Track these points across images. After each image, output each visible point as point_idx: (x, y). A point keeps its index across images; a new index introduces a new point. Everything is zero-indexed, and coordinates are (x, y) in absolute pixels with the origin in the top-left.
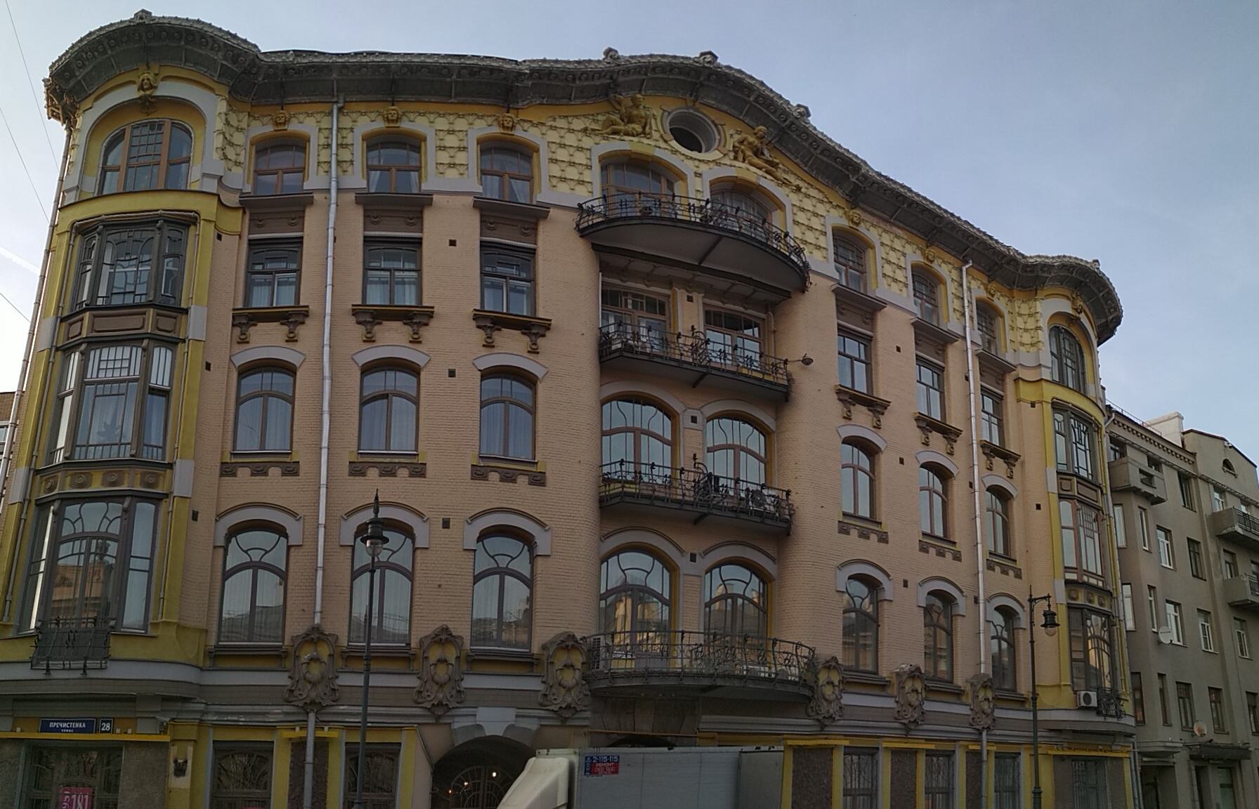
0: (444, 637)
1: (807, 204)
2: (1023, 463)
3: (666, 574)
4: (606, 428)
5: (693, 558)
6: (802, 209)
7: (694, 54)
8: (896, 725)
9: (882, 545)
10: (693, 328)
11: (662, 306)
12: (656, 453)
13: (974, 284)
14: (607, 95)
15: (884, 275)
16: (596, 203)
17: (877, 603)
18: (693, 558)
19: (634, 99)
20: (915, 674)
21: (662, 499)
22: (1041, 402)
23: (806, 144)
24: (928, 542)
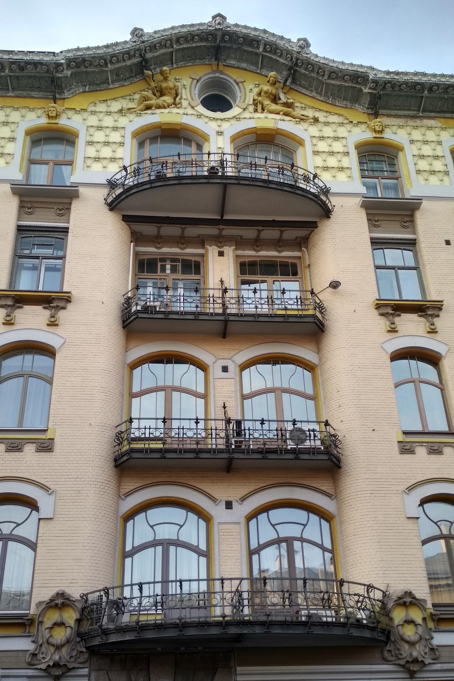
0: (408, 600)
1: (328, 132)
4: (246, 391)
5: (229, 505)
7: (207, 19)
11: (294, 266)
12: (187, 408)
14: (143, 73)
15: (418, 172)
18: (229, 505)
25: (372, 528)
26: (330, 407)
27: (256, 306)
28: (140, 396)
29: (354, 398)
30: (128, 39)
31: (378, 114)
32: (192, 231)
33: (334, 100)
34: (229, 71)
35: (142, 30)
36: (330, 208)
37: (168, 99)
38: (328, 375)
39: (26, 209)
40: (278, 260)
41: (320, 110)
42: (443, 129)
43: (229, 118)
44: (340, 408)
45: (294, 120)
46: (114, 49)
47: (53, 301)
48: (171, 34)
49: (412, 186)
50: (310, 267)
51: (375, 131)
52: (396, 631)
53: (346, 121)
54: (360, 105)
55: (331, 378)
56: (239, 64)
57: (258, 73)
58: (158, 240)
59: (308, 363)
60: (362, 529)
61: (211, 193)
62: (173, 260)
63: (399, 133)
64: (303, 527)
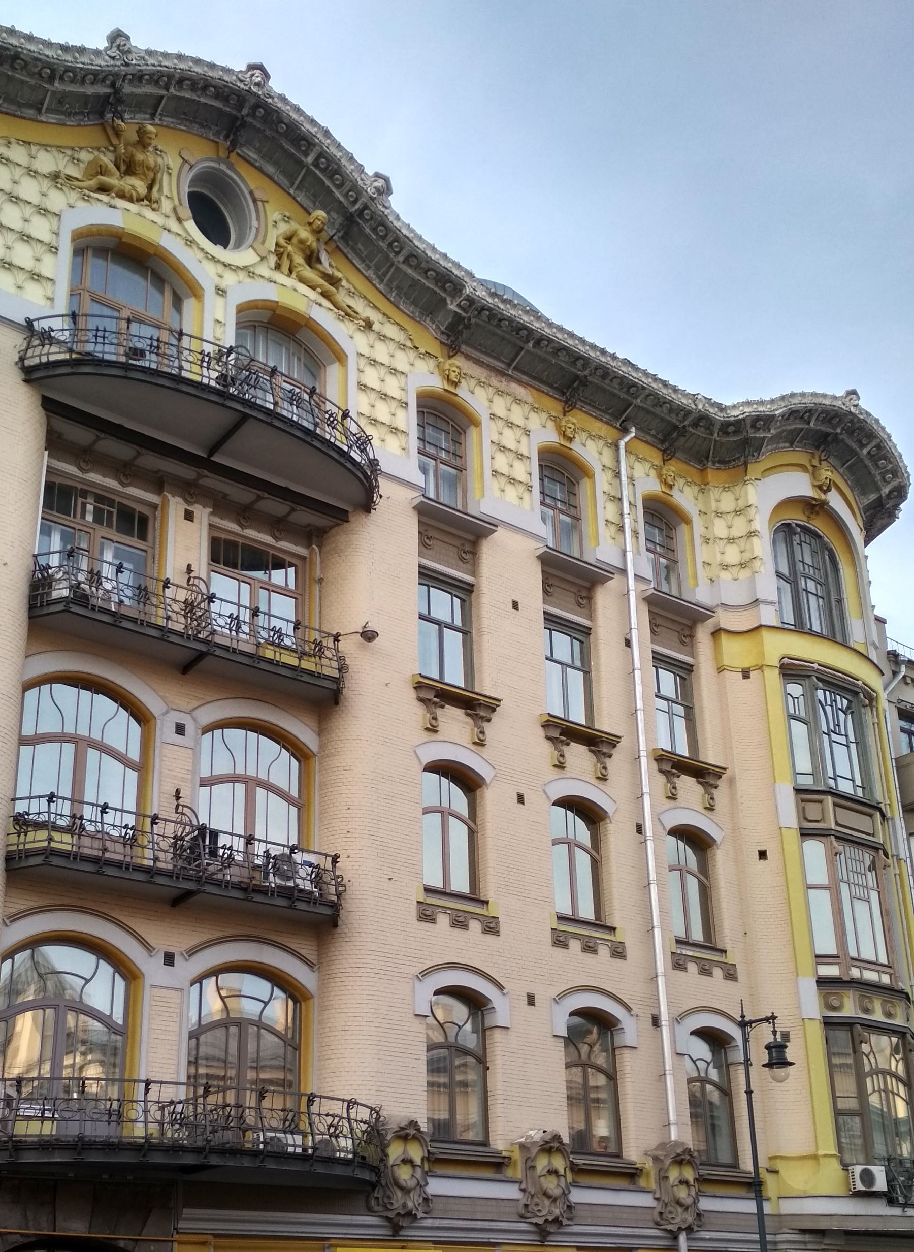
1: (381, 352)
2: (732, 782)
3: (120, 984)
5: (169, 959)
6: (373, 362)
7: (238, 65)
8: (523, 1226)
9: (490, 938)
10: (189, 569)
11: (144, 521)
12: (112, 786)
13: (640, 470)
15: (495, 473)
16: (57, 324)
17: (483, 1031)
18: (169, 959)
19: (141, 132)
20: (551, 1145)
21: (118, 865)
22: (760, 668)
23: (383, 245)
24: (570, 930)
25: (371, 1024)
26: (330, 830)
28: (34, 744)
29: (371, 825)
30: (101, 48)
31: (459, 351)
32: (151, 461)
33: (398, 298)
34: (244, 170)
37: (139, 185)
38: (335, 777)
40: (271, 552)
41: (375, 307)
42: (534, 409)
43: (238, 267)
44: (349, 835)
45: (336, 310)
46: (75, 58)
48: (175, 68)
49: (483, 496)
50: (324, 584)
51: (448, 379)
52: (390, 1172)
53: (409, 344)
54: (434, 323)
55: (340, 784)
56: (262, 162)
57: (290, 194)
59: (302, 746)
60: (357, 1023)
62: (99, 499)
63: (480, 396)
64: (262, 1005)
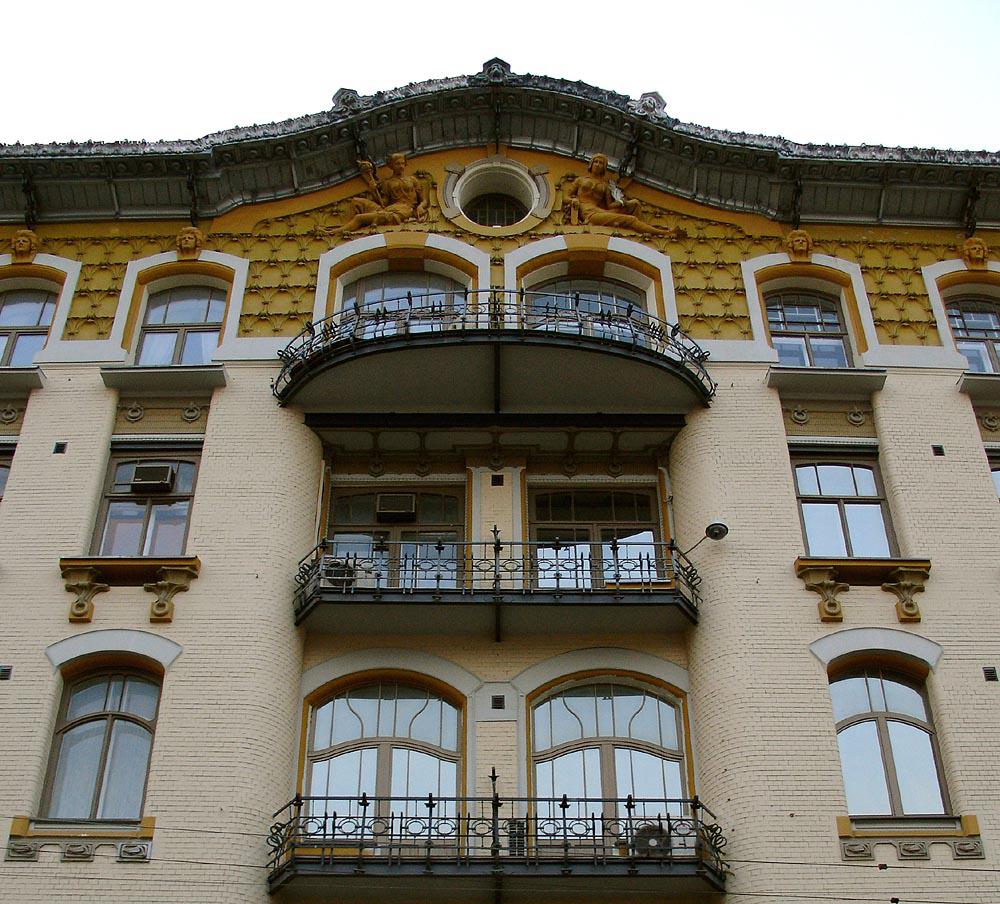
1: (704, 254)
27: (558, 575)
32: (441, 440)
35: (355, 92)
36: (709, 389)
37: (402, 208)
39: (130, 413)
47: (164, 577)
53: (739, 236)
58: (376, 459)
61: (475, 362)
